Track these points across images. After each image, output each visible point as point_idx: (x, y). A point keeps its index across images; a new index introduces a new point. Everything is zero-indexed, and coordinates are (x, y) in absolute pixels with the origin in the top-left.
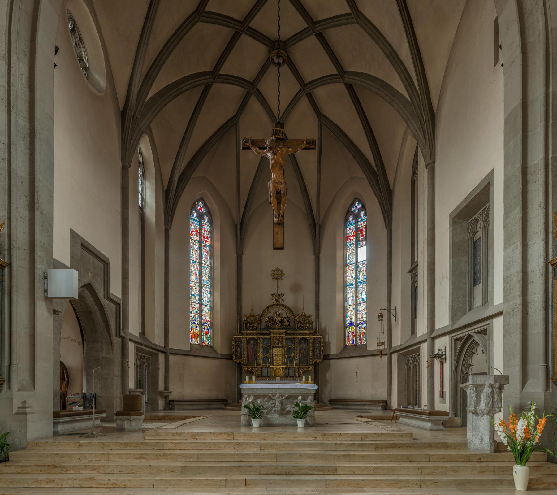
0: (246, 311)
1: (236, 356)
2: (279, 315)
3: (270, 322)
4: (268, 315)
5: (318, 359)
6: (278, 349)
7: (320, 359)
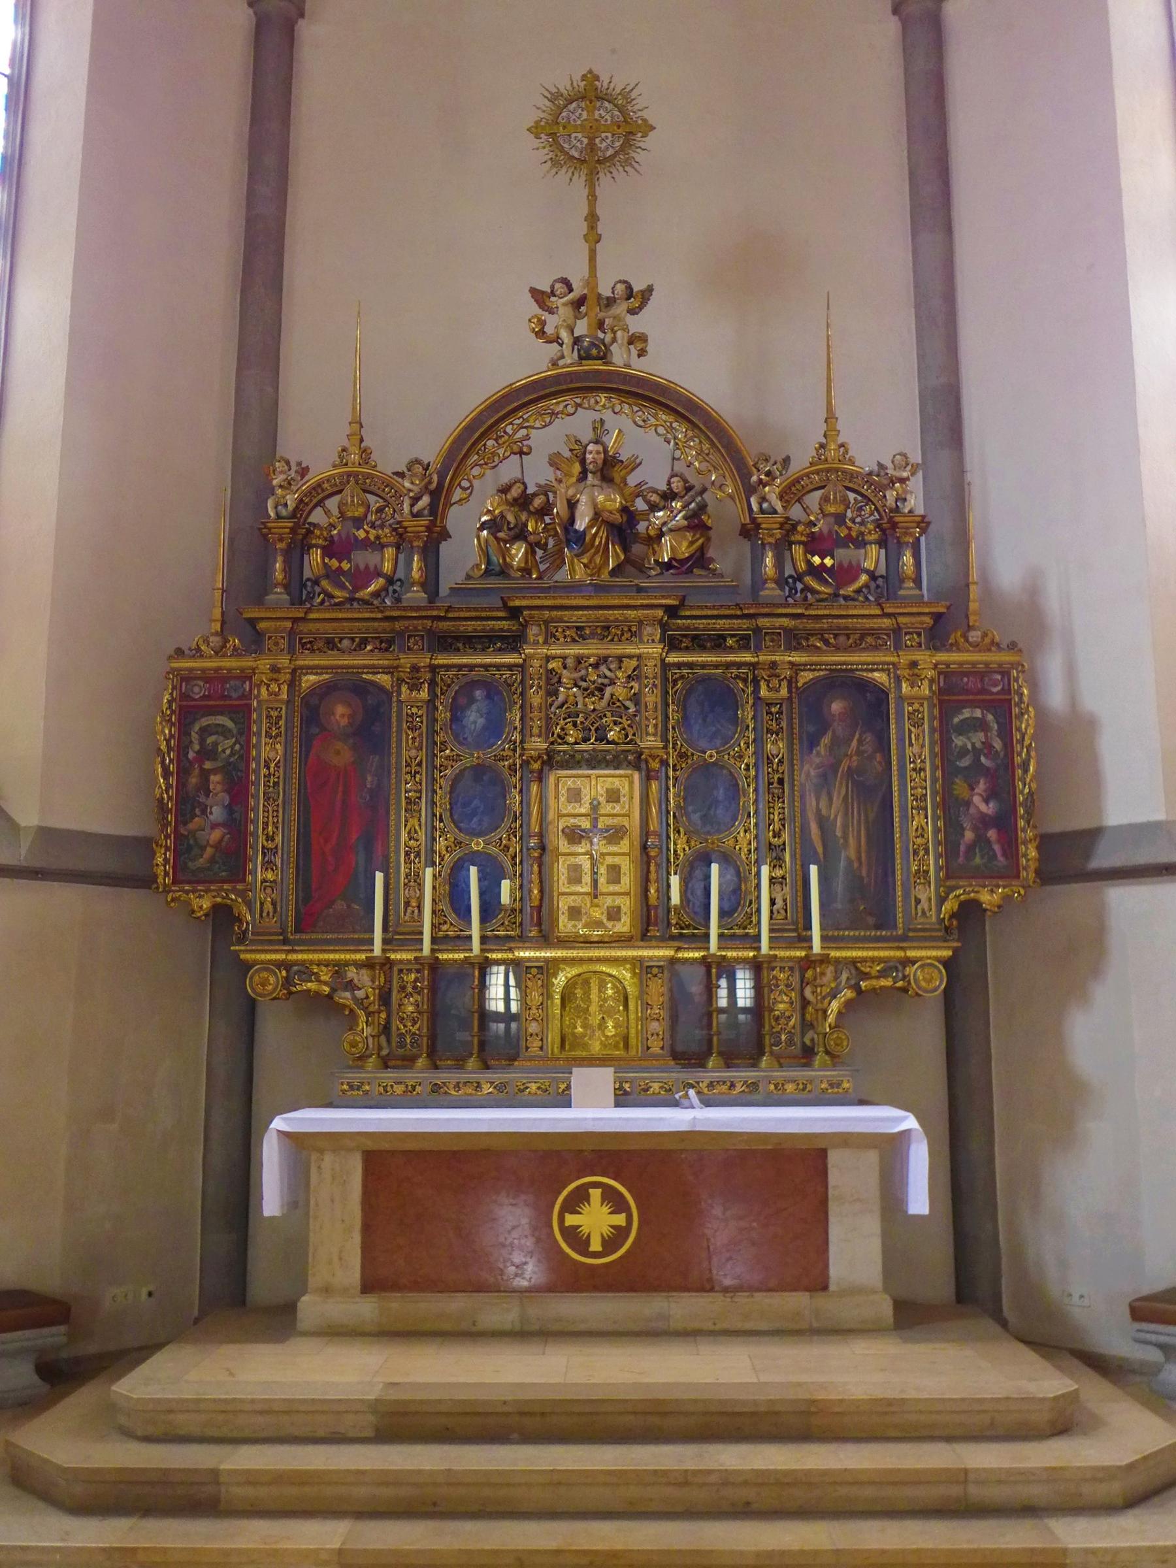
0: (312, 439)
1: (184, 848)
2: (609, 470)
3: (520, 534)
4: (509, 470)
5: (990, 875)
6: (596, 784)
7: (1012, 873)
